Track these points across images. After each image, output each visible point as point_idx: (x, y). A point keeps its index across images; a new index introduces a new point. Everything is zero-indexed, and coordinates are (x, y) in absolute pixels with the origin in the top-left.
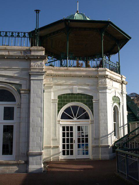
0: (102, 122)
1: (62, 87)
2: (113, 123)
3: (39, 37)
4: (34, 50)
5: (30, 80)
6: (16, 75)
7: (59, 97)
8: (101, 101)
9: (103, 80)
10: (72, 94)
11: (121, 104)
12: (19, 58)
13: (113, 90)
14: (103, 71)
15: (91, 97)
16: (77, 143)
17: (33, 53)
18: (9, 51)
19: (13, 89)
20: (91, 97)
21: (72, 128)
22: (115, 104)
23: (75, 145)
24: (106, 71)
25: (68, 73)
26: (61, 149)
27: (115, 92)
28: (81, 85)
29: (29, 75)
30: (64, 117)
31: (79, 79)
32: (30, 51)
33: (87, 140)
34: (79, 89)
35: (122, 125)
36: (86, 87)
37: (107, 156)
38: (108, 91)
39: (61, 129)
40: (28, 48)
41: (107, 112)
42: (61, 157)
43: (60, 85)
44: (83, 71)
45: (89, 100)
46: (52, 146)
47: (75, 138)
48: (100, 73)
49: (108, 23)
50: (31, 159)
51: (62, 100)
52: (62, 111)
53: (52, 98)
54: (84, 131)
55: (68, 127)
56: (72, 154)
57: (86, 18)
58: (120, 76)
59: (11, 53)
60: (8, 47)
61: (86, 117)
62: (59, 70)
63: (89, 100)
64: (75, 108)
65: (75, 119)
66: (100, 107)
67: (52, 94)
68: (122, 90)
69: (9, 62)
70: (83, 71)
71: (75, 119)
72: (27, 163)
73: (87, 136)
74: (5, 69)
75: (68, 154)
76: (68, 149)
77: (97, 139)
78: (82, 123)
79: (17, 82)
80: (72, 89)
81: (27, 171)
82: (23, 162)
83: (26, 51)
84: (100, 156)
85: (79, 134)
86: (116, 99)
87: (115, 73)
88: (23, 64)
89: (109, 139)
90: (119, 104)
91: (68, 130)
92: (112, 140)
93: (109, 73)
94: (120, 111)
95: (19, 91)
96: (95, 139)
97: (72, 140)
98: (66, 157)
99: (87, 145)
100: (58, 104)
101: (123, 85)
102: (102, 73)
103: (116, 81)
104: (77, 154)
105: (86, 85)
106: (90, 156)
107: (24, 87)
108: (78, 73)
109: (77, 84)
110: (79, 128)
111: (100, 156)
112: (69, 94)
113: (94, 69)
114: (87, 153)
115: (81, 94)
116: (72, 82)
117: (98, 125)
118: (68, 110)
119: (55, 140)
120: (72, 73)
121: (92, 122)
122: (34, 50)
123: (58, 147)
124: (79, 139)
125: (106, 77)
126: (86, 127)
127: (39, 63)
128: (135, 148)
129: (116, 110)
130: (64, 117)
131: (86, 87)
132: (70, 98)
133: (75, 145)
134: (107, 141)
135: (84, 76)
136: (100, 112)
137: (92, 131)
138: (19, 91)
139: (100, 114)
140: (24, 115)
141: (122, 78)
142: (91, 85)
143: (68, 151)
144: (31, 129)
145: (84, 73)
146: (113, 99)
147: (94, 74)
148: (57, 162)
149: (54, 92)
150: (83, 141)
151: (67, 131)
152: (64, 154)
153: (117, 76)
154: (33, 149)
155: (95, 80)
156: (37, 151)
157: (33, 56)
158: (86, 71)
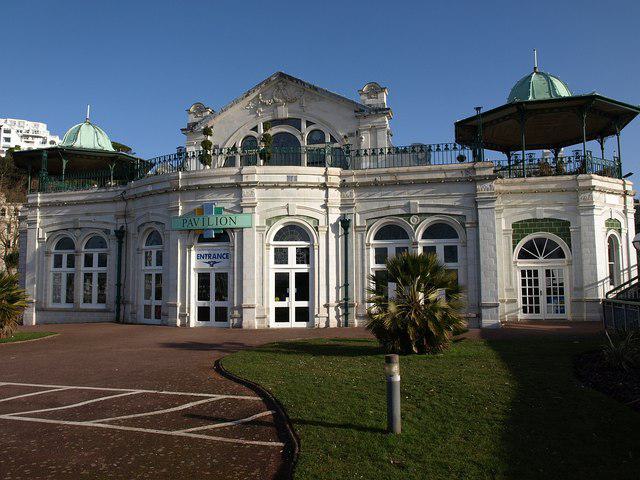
0: (586, 263)
1: (519, 210)
2: (608, 263)
3: (473, 133)
4: (480, 169)
5: (477, 209)
6: (457, 204)
7: (514, 226)
8: (584, 229)
9: (587, 195)
10: (536, 220)
11: (624, 232)
12: (460, 181)
13: (607, 208)
14: (586, 179)
15: (568, 223)
16: (546, 296)
17: (478, 173)
18: (445, 171)
19: (455, 223)
20: (568, 223)
21: (536, 272)
22: (612, 232)
23: (543, 298)
24: (594, 193)
25: (527, 187)
26: (520, 304)
27: (608, 203)
28: (547, 206)
29: (475, 203)
30: (523, 255)
31: (545, 195)
32: (474, 169)
33: (562, 291)
34: (546, 211)
35: (626, 267)
36: (557, 208)
37: (597, 316)
38: (595, 212)
39: (519, 274)
40: (470, 165)
41: (595, 246)
42: (521, 316)
43: (515, 206)
44: (552, 182)
45: (563, 228)
46: (506, 299)
47: (542, 287)
48: (581, 184)
49: (592, 97)
50: (484, 311)
51: (519, 229)
52: (520, 246)
53: (504, 228)
54: (556, 277)
55: (529, 272)
56: (538, 311)
57: (552, 88)
58: (621, 181)
59: (449, 175)
60: (444, 167)
61: (560, 254)
62: (512, 184)
63: (563, 228)
64: (540, 242)
65: (541, 259)
66: (584, 239)
67: (503, 220)
68: (625, 207)
69: (447, 186)
70: (552, 182)
71: (541, 259)
72: (479, 316)
73: (561, 284)
74: (443, 197)
75: (531, 311)
76: (531, 303)
77: (579, 288)
78: (553, 264)
79: (460, 213)
80: (534, 212)
81: (480, 327)
82: (474, 315)
83: (467, 171)
84: (396, 368)
85: (548, 281)
86: (612, 223)
87: (610, 179)
88: (467, 188)
89: (600, 290)
90: (620, 231)
91: (530, 275)
92: (604, 290)
93: (597, 181)
94: (622, 243)
95: (463, 225)
96: (576, 289)
97: (537, 291)
98: (528, 316)
99: (562, 299)
100: (514, 237)
101: (628, 197)
102: (586, 184)
103: (612, 193)
104: (545, 312)
105: (556, 204)
106: (568, 315)
107: (469, 220)
108: (543, 187)
109: (542, 205)
110: (548, 273)
111: (396, 368)
112: (529, 220)
113: (570, 177)
114: (563, 311)
115: (550, 219)
116: (533, 201)
117: (582, 268)
118: (529, 245)
119: (509, 290)
120: (533, 187)
121: (570, 263)
122: (480, 169)
123: (515, 301)
124: (548, 290)
125: (591, 189)
126: (560, 272)
127: (487, 185)
128: (260, 307)
129: (613, 244)
130: (523, 255)
131: (557, 208)
132: (531, 225)
133: (543, 298)
134: (597, 291)
135: (554, 191)
136: (583, 246)
137: (571, 276)
138: (463, 225)
139: (584, 250)
140: (471, 255)
141: (624, 185)
142: (569, 204)
143: (531, 308)
144: (482, 273)
145: (553, 186)
146: (607, 224)
147: (572, 185)
148: (516, 321)
149: (506, 218)
150: (556, 292)
151: (529, 276)
152: (525, 311)
153: (615, 184)
154: (485, 300)
155: (573, 195)
156: (492, 302)
157: (480, 176)
158: (556, 182)
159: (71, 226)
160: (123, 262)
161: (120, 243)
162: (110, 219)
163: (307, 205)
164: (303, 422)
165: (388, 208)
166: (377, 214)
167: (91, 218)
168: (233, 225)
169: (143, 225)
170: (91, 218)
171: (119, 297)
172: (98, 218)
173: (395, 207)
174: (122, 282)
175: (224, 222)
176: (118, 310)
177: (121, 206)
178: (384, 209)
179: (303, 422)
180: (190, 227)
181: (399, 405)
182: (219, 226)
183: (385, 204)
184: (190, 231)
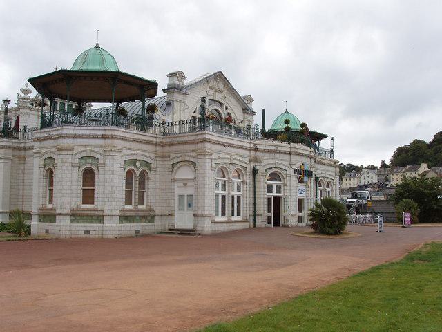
169: (271, 169)
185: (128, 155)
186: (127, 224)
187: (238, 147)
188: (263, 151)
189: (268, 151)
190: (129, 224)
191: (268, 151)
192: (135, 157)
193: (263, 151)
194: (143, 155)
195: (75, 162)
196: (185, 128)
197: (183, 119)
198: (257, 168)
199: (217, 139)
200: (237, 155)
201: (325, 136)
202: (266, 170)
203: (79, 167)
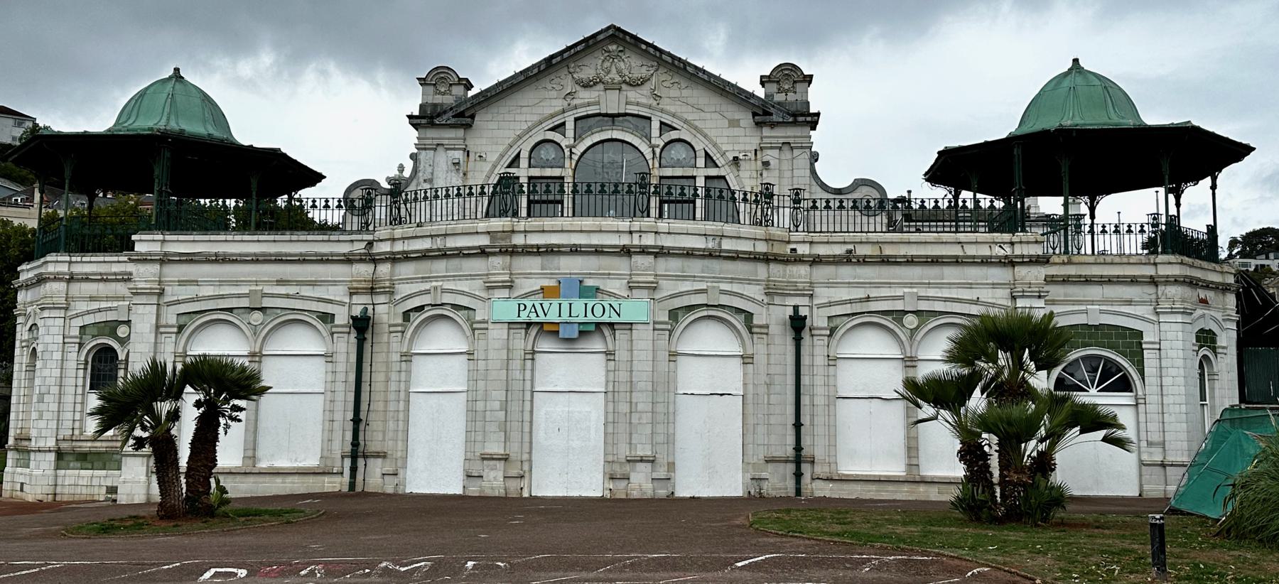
61: (1124, 385)
65: (1093, 391)
146: (1198, 339)
159: (245, 303)
160: (366, 377)
161: (361, 342)
162: (339, 293)
163: (736, 288)
164: (1214, 187)
165: (868, 299)
166: (848, 309)
167: (292, 290)
168: (615, 319)
169: (420, 309)
170: (292, 290)
171: (355, 443)
172: (306, 291)
173: (877, 299)
174: (363, 416)
175: (598, 310)
176: (354, 470)
177: (364, 270)
178: (861, 300)
179: (1214, 187)
180: (534, 318)
181: (1105, 273)
182: (590, 318)
183: (860, 293)
184: (529, 324)
185: (88, 313)
186: (83, 472)
187: (279, 259)
188: (394, 258)
189: (406, 257)
190: (90, 472)
191: (406, 257)
192: (111, 316)
193: (394, 258)
194: (1101, 312)
195: (72, 334)
196: (1133, 244)
197: (1126, 219)
198: (803, 312)
199: (903, 251)
200: (281, 282)
201: (1238, 151)
202: (406, 315)
203: (81, 345)
